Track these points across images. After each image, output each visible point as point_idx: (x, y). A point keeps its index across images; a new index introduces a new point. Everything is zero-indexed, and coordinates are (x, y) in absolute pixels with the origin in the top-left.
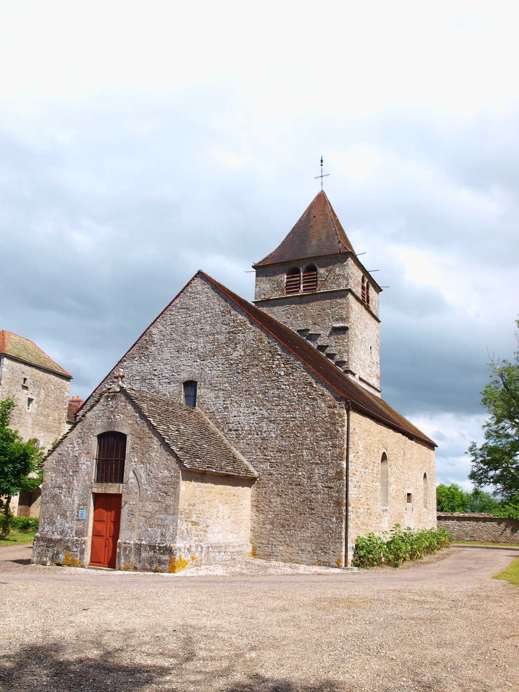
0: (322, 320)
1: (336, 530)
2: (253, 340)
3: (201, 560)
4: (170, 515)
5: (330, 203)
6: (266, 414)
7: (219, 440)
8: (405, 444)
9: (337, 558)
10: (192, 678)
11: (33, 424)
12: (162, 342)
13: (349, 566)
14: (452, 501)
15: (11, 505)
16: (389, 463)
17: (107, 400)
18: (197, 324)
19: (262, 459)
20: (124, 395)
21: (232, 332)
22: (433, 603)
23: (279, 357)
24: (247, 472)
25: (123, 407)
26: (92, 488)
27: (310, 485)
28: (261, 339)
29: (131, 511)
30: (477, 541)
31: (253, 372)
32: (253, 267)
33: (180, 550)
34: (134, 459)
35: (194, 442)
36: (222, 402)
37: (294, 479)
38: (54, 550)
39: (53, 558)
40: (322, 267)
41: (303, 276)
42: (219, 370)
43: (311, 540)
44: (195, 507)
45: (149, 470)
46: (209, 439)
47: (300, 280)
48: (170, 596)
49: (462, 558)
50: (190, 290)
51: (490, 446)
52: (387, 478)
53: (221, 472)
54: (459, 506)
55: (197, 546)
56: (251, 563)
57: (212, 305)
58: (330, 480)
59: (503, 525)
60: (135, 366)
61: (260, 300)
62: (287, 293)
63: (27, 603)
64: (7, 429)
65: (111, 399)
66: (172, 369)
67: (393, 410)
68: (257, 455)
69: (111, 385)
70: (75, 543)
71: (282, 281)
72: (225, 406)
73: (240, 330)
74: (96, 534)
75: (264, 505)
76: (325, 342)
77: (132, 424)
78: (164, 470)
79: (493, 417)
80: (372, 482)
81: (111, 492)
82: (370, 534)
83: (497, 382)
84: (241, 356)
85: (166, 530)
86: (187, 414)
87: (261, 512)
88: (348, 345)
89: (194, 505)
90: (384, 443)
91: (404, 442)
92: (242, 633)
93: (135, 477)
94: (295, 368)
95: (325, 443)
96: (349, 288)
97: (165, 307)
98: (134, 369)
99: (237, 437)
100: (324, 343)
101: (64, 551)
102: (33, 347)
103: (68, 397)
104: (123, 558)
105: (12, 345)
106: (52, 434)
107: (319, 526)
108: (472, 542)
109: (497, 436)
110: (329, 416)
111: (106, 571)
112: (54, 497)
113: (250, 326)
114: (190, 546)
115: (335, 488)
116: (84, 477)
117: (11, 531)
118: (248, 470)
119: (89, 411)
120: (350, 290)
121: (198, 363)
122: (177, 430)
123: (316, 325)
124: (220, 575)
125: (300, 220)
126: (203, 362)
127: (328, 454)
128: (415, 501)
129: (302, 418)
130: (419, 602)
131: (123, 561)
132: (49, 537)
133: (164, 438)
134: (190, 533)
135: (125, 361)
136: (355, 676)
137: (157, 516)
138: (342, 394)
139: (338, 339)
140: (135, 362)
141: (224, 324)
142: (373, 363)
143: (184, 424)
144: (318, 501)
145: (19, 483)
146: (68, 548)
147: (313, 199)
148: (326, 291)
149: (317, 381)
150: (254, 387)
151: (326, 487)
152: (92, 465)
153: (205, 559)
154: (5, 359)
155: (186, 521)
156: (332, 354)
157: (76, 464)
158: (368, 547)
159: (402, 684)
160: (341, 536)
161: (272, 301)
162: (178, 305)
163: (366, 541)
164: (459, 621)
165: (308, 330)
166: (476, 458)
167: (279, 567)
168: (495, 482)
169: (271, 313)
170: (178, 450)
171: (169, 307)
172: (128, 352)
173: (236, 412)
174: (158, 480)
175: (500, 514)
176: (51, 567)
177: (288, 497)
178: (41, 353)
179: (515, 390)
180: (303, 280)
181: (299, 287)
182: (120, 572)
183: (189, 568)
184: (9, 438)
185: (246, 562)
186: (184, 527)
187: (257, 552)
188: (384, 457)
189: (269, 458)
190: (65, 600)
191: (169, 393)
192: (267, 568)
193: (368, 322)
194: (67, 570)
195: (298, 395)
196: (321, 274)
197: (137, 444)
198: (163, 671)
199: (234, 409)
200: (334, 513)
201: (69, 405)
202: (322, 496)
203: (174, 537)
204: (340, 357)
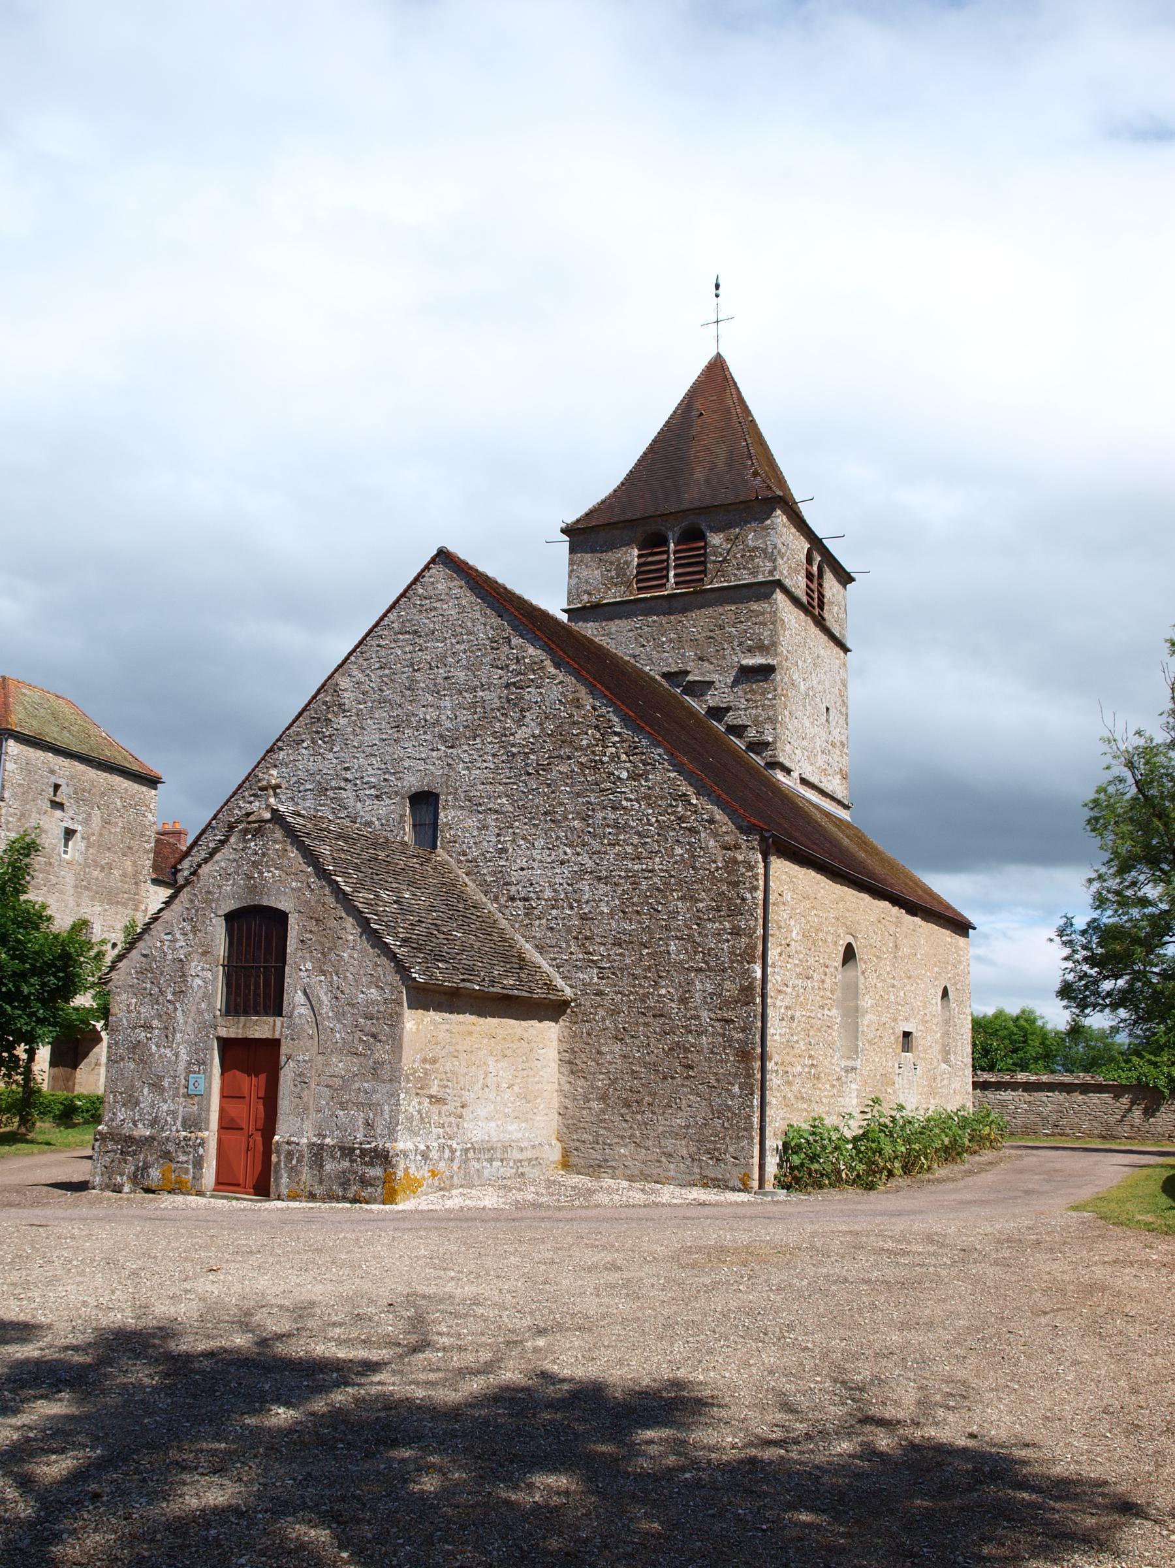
0: (718, 651)
1: (740, 1112)
2: (560, 701)
3: (452, 1177)
4: (384, 1082)
5: (735, 384)
6: (590, 864)
7: (488, 920)
8: (898, 924)
9: (743, 1171)
10: (422, 1377)
11: (76, 887)
12: (361, 707)
13: (769, 1187)
14: (1023, 1048)
15: (36, 1068)
16: (861, 966)
17: (244, 839)
18: (437, 667)
19: (580, 960)
20: (281, 826)
21: (514, 684)
22: (920, 1254)
23: (617, 739)
24: (548, 989)
25: (280, 853)
26: (215, 1027)
27: (685, 1017)
28: (578, 700)
29: (299, 1075)
30: (1068, 1135)
31: (561, 773)
32: (563, 531)
33: (406, 1155)
34: (304, 966)
35: (433, 927)
36: (494, 839)
37: (651, 1003)
38: (138, 1160)
39: (136, 1177)
40: (717, 530)
41: (675, 552)
42: (486, 768)
43: (687, 1134)
44: (437, 1065)
45: (338, 988)
46: (465, 919)
47: (667, 560)
48: (383, 1245)
49: (1021, 1171)
50: (421, 591)
51: (1105, 925)
52: (857, 998)
53: (492, 989)
54: (1036, 1060)
55: (442, 1148)
56: (559, 1182)
57: (469, 624)
58: (727, 1004)
59: (1125, 1100)
60: (304, 760)
61: (579, 605)
62: (639, 589)
63: (95, 1261)
64: (26, 902)
65: (253, 836)
66: (383, 766)
67: (877, 849)
68: (571, 953)
69: (251, 803)
70: (183, 1144)
71: (628, 563)
72: (500, 846)
73: (532, 681)
74: (227, 1125)
75: (585, 1059)
76: (725, 700)
77: (299, 889)
78: (369, 988)
79: (1112, 860)
80: (822, 1007)
81: (257, 1035)
82: (815, 1120)
83: (1121, 781)
84: (533, 736)
85: (375, 1115)
86: (417, 866)
87: (580, 1074)
88: (774, 706)
89: (434, 1061)
90: (849, 923)
91: (894, 919)
92: (522, 1308)
93: (308, 1003)
94: (650, 764)
95: (717, 925)
96: (777, 577)
97: (367, 630)
98: (301, 767)
99: (526, 915)
100: (722, 702)
101: (159, 1162)
102: (72, 713)
103: (155, 823)
104: (286, 1175)
105: (25, 709)
106: (120, 909)
107: (705, 1103)
108: (1056, 1138)
109: (1119, 903)
110: (726, 867)
111: (249, 1203)
112: (134, 1048)
113: (552, 670)
114: (428, 1147)
115: (739, 1022)
116: (199, 1004)
117: (38, 1124)
118: (551, 985)
119: (206, 863)
120: (779, 584)
121: (441, 753)
122: (396, 902)
123: (703, 661)
124: (490, 1207)
125: (667, 422)
126: (451, 750)
127: (723, 949)
128: (920, 1048)
129: (666, 871)
130: (890, 1252)
131: (284, 1180)
132: (126, 1132)
133: (368, 920)
134: (427, 1120)
135: (281, 749)
136: (727, 1375)
137: (357, 1085)
138: (753, 820)
139: (753, 692)
140: (304, 751)
141: (497, 667)
142: (833, 745)
143: (410, 888)
144: (702, 1051)
145: (55, 1017)
146: (167, 1155)
147: (698, 374)
148: (726, 584)
149: (698, 792)
150: (562, 804)
151: (718, 1020)
152: (216, 978)
153: (460, 1175)
154: (11, 742)
155: (417, 1094)
156: (740, 726)
157: (181, 977)
158: (810, 1148)
159: (812, 1386)
160: (751, 1123)
161: (607, 609)
162: (395, 625)
163: (806, 1135)
164: (961, 1286)
165: (687, 673)
166: (1074, 951)
167: (618, 1190)
168: (1114, 1007)
169: (603, 635)
170: (398, 943)
171: (376, 629)
172: (288, 729)
173: (525, 860)
174: (358, 1008)
175: (1119, 1077)
176: (132, 1196)
177: (637, 1042)
178: (91, 727)
179: (1162, 798)
180: (674, 561)
181: (667, 577)
182: (279, 1204)
183: (426, 1194)
184: (35, 919)
185: (548, 1180)
186: (414, 1107)
187: (573, 1160)
188: (849, 954)
189: (595, 958)
190: (171, 1254)
191: (378, 819)
192: (591, 1192)
193: (822, 652)
194: (168, 1201)
195: (657, 821)
196: (714, 546)
197: (311, 931)
198: (371, 1367)
199: (520, 853)
200: (736, 1074)
201: (156, 841)
202: (710, 1039)
203: (394, 1129)
204: (757, 732)
